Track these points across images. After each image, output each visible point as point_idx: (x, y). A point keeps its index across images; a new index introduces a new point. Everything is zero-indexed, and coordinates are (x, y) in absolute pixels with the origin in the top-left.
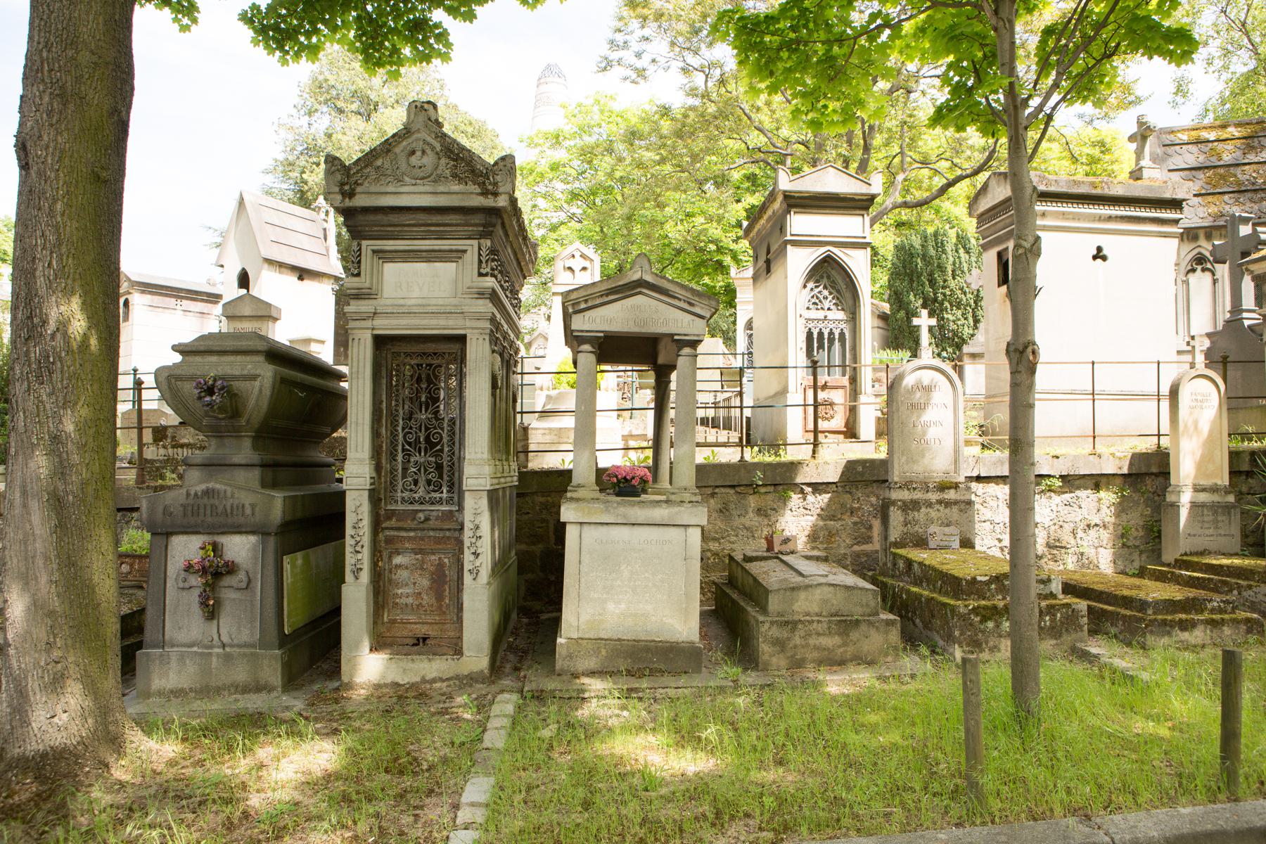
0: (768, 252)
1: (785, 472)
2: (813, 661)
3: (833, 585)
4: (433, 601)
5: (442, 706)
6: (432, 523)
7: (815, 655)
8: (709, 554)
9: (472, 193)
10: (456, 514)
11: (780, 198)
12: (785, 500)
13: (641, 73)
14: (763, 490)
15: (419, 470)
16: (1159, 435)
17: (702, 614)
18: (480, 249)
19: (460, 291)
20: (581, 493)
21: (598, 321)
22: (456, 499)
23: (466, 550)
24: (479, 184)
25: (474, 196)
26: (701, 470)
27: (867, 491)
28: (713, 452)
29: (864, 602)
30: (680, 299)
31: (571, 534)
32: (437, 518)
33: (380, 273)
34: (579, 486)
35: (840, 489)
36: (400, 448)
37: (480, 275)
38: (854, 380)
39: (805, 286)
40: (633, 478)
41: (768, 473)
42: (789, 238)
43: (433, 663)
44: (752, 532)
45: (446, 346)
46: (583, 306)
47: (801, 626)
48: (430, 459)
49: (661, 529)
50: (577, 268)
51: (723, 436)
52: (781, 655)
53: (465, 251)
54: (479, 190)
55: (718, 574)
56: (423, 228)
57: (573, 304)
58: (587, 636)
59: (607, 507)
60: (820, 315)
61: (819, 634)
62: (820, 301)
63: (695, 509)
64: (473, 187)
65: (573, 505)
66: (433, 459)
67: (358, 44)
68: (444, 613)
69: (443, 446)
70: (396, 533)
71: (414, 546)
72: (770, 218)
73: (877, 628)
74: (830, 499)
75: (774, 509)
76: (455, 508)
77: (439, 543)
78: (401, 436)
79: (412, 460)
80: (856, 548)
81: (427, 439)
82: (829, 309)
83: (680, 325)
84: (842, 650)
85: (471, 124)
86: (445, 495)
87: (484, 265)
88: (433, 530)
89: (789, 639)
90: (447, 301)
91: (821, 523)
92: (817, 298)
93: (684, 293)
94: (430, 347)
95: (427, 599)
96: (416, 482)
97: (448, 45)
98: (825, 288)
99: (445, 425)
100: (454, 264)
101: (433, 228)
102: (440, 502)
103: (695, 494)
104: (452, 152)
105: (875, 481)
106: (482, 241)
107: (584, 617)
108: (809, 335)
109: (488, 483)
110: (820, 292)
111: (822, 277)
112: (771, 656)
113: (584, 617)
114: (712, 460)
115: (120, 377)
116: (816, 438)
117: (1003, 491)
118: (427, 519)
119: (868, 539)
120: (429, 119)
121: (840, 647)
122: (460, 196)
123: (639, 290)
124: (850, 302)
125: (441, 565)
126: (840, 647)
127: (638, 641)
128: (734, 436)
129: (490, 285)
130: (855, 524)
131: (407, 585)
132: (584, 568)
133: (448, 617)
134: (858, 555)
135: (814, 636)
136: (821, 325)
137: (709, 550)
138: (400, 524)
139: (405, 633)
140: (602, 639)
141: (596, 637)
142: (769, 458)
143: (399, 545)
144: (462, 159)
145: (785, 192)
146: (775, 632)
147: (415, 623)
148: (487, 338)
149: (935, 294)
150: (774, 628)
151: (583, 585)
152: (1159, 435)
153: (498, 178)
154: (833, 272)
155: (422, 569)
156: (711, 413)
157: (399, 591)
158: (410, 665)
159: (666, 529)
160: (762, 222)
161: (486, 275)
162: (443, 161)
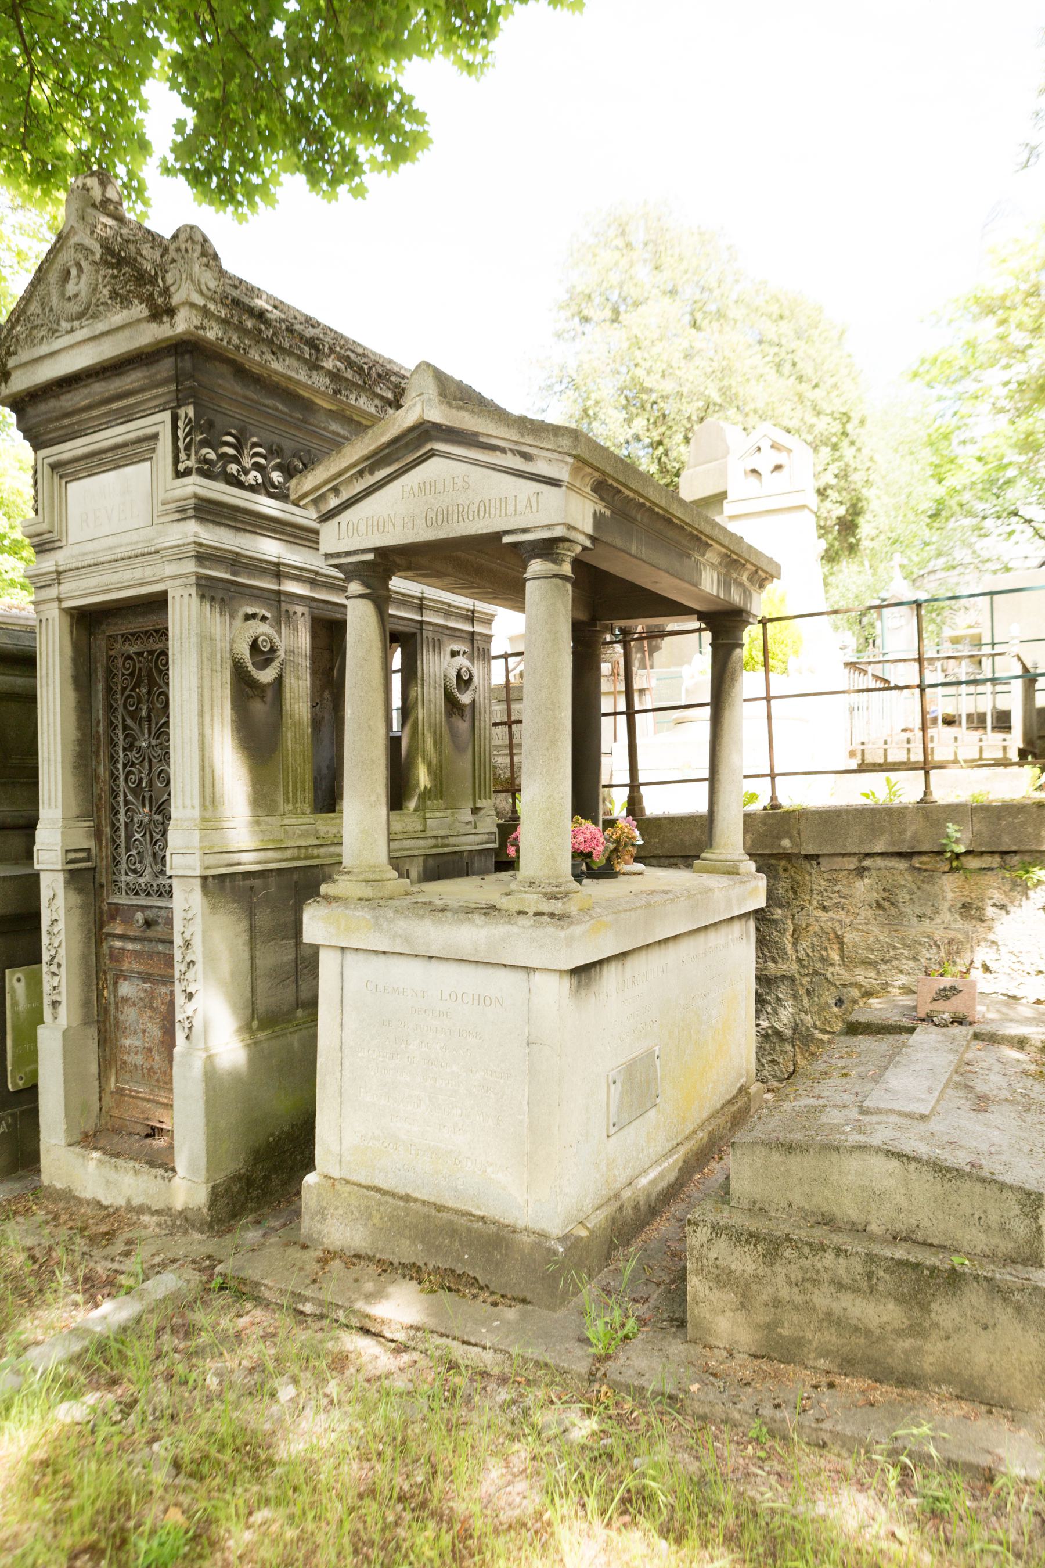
3: (899, 1156)
7: (831, 1337)
14: (973, 863)
16: (773, 776)
21: (362, 528)
25: (144, 326)
28: (888, 780)
29: (993, 1218)
30: (503, 450)
31: (328, 965)
33: (63, 501)
36: (121, 799)
37: (178, 475)
46: (333, 502)
50: (765, 469)
53: (155, 437)
56: (103, 410)
57: (315, 502)
58: (354, 1178)
59: (376, 918)
61: (840, 1286)
63: (539, 932)
67: (50, 127)
71: (142, 968)
73: (1019, 1309)
75: (1003, 907)
83: (511, 509)
84: (907, 1343)
87: (183, 456)
89: (758, 1279)
100: (148, 464)
101: (114, 406)
115: (708, 700)
121: (900, 1333)
122: (127, 333)
123: (428, 447)
126: (900, 1333)
127: (440, 1208)
135: (825, 1287)
137: (856, 985)
140: (378, 1190)
148: (193, 591)
150: (722, 1243)
152: (773, 776)
155: (151, 1007)
159: (490, 971)
161: (187, 472)
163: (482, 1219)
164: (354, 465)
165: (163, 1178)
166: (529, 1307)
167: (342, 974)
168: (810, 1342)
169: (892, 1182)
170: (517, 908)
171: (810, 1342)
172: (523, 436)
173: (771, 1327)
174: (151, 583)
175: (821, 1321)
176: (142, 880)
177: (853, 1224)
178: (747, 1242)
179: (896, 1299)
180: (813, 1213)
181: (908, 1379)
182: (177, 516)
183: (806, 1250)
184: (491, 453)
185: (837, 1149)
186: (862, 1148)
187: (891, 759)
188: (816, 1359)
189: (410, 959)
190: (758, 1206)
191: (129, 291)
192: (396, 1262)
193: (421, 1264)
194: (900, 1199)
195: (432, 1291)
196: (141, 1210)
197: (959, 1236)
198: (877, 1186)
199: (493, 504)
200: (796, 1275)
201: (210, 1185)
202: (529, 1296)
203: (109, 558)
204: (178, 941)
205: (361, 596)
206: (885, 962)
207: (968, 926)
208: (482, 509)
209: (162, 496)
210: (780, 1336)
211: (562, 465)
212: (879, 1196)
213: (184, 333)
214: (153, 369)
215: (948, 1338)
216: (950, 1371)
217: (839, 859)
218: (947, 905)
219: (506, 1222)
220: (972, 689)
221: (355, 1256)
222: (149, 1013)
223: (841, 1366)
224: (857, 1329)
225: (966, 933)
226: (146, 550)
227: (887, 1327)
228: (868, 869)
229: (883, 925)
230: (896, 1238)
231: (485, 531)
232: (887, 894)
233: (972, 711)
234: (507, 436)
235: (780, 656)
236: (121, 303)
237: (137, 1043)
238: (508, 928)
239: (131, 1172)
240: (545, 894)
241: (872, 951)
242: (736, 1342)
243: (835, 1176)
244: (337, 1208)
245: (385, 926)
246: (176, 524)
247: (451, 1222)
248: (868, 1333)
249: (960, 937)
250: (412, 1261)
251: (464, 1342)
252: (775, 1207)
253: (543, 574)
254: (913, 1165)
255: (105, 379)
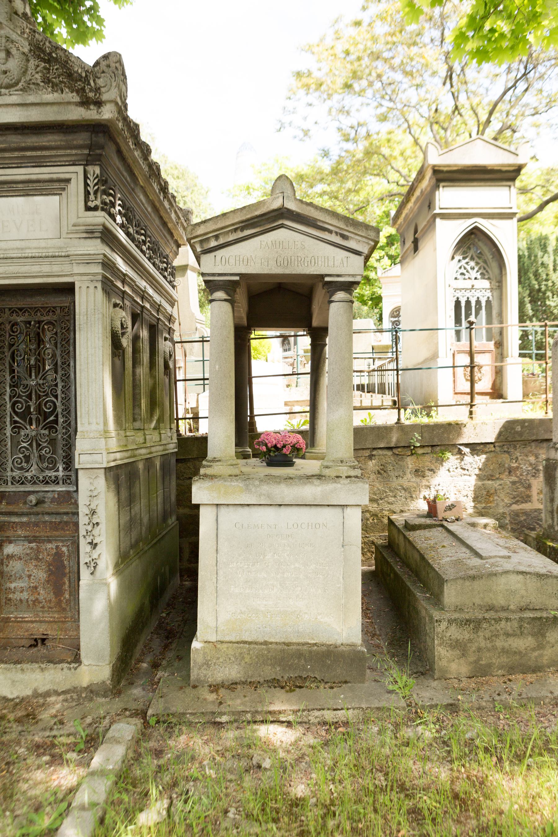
0: (416, 232)
1: (443, 433)
2: (501, 667)
3: (522, 573)
4: (52, 596)
5: (47, 733)
6: (47, 506)
7: (504, 659)
8: (368, 515)
9: (69, 103)
10: (75, 494)
11: (429, 174)
12: (441, 461)
13: (306, 133)
14: (420, 451)
15: (31, 445)
17: (365, 575)
18: (86, 178)
19: (64, 230)
20: (216, 469)
21: (232, 261)
22: (73, 478)
23: (81, 539)
24: (77, 92)
25: (73, 107)
26: (359, 432)
27: (526, 450)
28: (369, 414)
30: (330, 232)
32: (53, 500)
34: (214, 460)
35: (498, 449)
37: (88, 209)
38: (500, 345)
39: (453, 258)
40: (284, 446)
41: (425, 435)
42: (437, 211)
43: (47, 674)
44: (410, 492)
45: (57, 299)
46: (213, 243)
47: (485, 625)
48: (43, 432)
49: (314, 510)
51: (377, 399)
52: (462, 661)
53: (68, 181)
54: (77, 99)
55: (377, 534)
56: (16, 154)
57: (201, 242)
58: (227, 639)
59: (247, 486)
60: (468, 284)
61: (508, 635)
62: (467, 271)
63: (353, 486)
64: (70, 95)
65: (207, 484)
66: (46, 432)
68: (64, 610)
69: (57, 416)
70: (6, 519)
71: (27, 533)
72: (418, 199)
74: (487, 459)
75: (432, 470)
76: (72, 488)
77: (57, 529)
78: (8, 406)
79: (22, 433)
80: (515, 507)
81: (39, 409)
82: (476, 279)
83: (331, 263)
84: (536, 654)
85: (176, 168)
86: (61, 473)
87: (92, 197)
88: (48, 514)
89: (470, 641)
90: (50, 243)
91: (480, 483)
92: (465, 268)
93: (334, 222)
94: (38, 301)
95: (44, 594)
96: (27, 459)
97: (100, 21)
98: (472, 259)
99: (59, 392)
100: (57, 197)
101: (29, 154)
102: (56, 481)
103: (354, 468)
104: (44, 52)
105: (534, 441)
106: (90, 168)
107: (224, 617)
108: (458, 303)
109: (105, 460)
110: (467, 263)
111: (469, 248)
112: (449, 661)
113: (224, 617)
114: (370, 423)
116: (472, 399)
117: (178, 379)
118: (39, 502)
119: (527, 499)
120: (16, 13)
121: (534, 650)
122: (55, 108)
123: (280, 222)
124: (496, 271)
125: (58, 555)
126: (534, 650)
127: (288, 644)
128: (388, 400)
129: (100, 220)
130: (514, 483)
131: (21, 578)
132: (222, 558)
133: (69, 614)
134: (517, 514)
135: (501, 637)
136: (468, 294)
138: (11, 508)
139: (21, 633)
140: (245, 642)
141: (238, 639)
142: (425, 420)
143: (10, 533)
144: (56, 60)
145: (434, 166)
146: (454, 632)
147: (32, 622)
148: (99, 285)
149: (540, 285)
150: (453, 628)
151: (221, 578)
153: (100, 82)
154: (480, 244)
155: (37, 559)
156: (365, 381)
157: (13, 586)
158: (20, 676)
159: (319, 509)
160: (410, 205)
161: (95, 209)
162: (33, 63)
163: (315, 644)
164: (233, 225)
165: (70, 669)
166: (349, 685)
167: (217, 520)
168: (495, 664)
169: (519, 585)
170: (335, 474)
171: (495, 664)
172: (347, 226)
173: (476, 662)
174: (59, 276)
175: (499, 653)
176: (28, 475)
177: (503, 607)
178: (466, 624)
179: (532, 635)
180: (485, 606)
181: (536, 669)
182: (85, 235)
183: (493, 622)
184: (321, 232)
185: (495, 575)
186: (507, 572)
187: (374, 404)
188: (497, 671)
189: (266, 508)
190: (459, 607)
191: (61, 82)
192: (262, 680)
193: (279, 678)
194: (523, 592)
195: (291, 691)
196: (48, 694)
197: (547, 603)
198: (513, 588)
199: (320, 259)
200: (488, 634)
201: (111, 665)
202: (348, 679)
203: (20, 255)
204: (83, 510)
205: (225, 300)
206: (381, 499)
207: (418, 480)
208: (313, 261)
209: (73, 220)
210: (481, 665)
211: (365, 244)
212: (513, 592)
213: (108, 120)
214: (70, 137)
215: (553, 647)
216: (554, 661)
217: (361, 451)
218: (409, 470)
219: (331, 643)
220: (358, 374)
221: (232, 684)
222: (34, 563)
223: (508, 671)
224: (515, 652)
225: (417, 483)
226: (57, 254)
227: (529, 648)
228: (375, 455)
229: (380, 482)
230: (522, 610)
231: (315, 273)
232: (382, 467)
233: (359, 383)
234: (338, 225)
235: (263, 353)
236: (53, 87)
237: (22, 585)
238: (335, 485)
239: (38, 670)
240: (350, 467)
241: (375, 494)
242: (460, 673)
243: (495, 587)
244: (218, 658)
245: (253, 490)
246: (82, 240)
247: (298, 650)
248: (520, 652)
249: (415, 485)
250: (273, 677)
251: (335, 710)
252: (467, 606)
253: (346, 299)
254: (529, 576)
255: (22, 134)
